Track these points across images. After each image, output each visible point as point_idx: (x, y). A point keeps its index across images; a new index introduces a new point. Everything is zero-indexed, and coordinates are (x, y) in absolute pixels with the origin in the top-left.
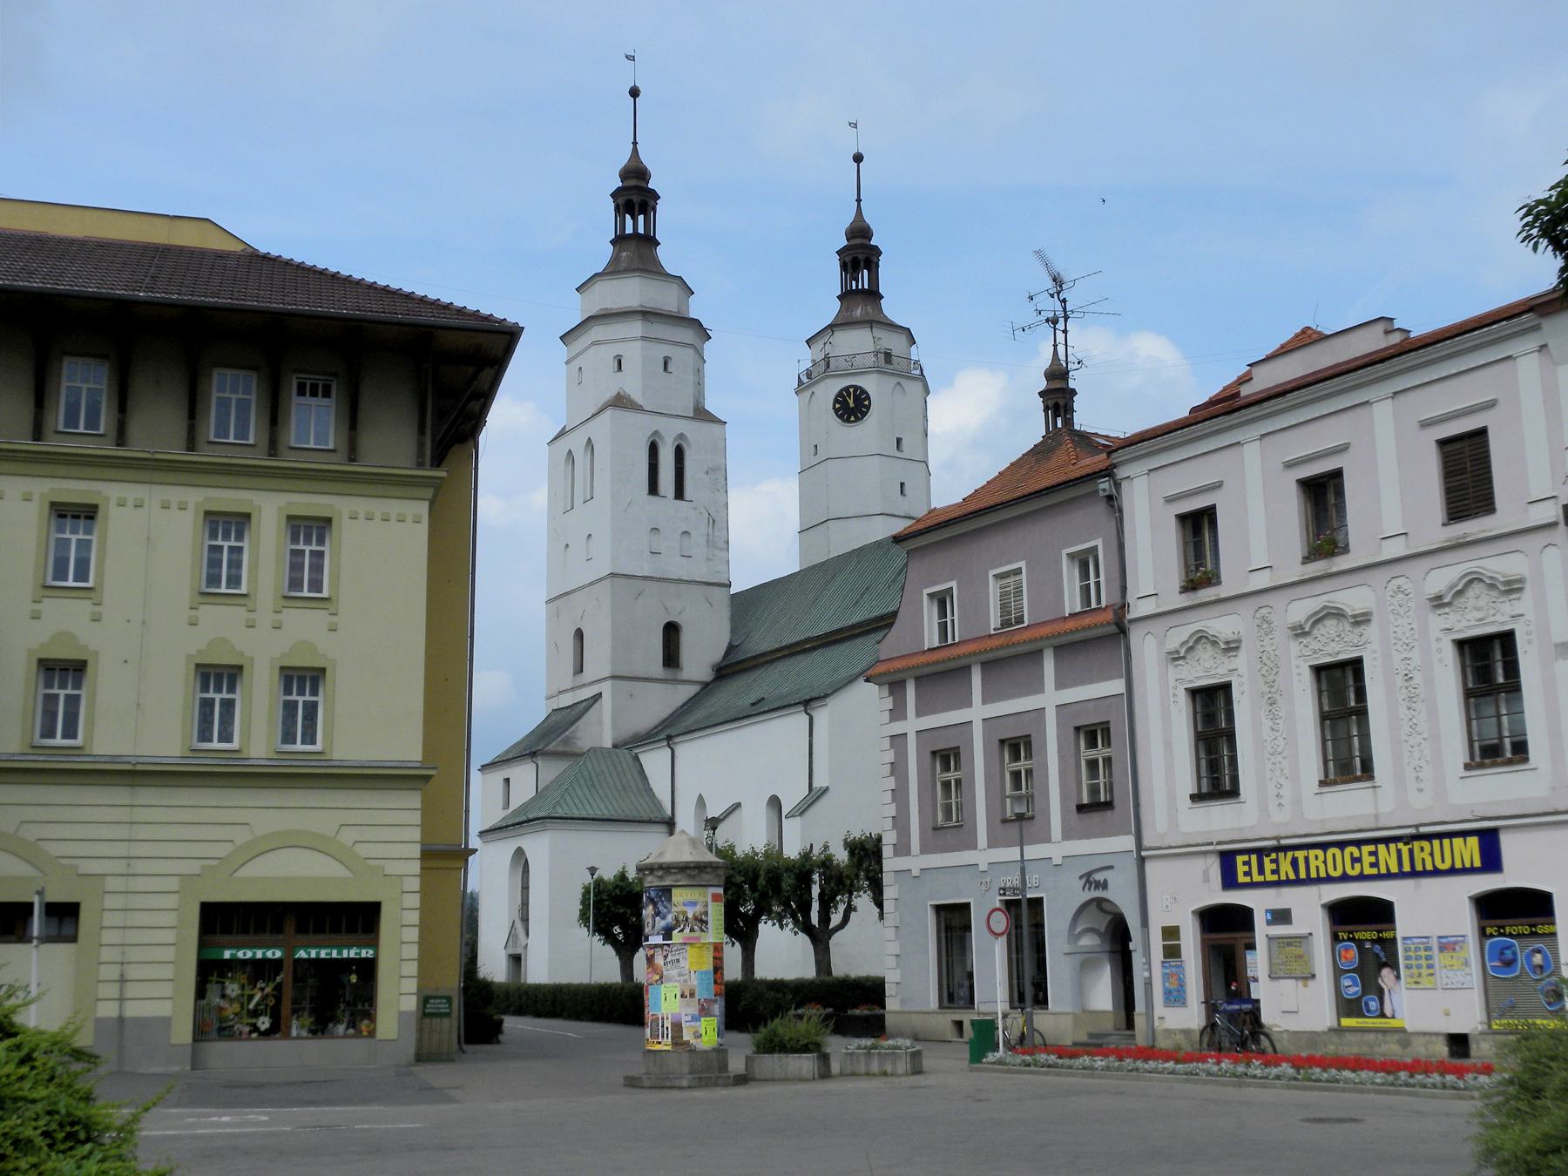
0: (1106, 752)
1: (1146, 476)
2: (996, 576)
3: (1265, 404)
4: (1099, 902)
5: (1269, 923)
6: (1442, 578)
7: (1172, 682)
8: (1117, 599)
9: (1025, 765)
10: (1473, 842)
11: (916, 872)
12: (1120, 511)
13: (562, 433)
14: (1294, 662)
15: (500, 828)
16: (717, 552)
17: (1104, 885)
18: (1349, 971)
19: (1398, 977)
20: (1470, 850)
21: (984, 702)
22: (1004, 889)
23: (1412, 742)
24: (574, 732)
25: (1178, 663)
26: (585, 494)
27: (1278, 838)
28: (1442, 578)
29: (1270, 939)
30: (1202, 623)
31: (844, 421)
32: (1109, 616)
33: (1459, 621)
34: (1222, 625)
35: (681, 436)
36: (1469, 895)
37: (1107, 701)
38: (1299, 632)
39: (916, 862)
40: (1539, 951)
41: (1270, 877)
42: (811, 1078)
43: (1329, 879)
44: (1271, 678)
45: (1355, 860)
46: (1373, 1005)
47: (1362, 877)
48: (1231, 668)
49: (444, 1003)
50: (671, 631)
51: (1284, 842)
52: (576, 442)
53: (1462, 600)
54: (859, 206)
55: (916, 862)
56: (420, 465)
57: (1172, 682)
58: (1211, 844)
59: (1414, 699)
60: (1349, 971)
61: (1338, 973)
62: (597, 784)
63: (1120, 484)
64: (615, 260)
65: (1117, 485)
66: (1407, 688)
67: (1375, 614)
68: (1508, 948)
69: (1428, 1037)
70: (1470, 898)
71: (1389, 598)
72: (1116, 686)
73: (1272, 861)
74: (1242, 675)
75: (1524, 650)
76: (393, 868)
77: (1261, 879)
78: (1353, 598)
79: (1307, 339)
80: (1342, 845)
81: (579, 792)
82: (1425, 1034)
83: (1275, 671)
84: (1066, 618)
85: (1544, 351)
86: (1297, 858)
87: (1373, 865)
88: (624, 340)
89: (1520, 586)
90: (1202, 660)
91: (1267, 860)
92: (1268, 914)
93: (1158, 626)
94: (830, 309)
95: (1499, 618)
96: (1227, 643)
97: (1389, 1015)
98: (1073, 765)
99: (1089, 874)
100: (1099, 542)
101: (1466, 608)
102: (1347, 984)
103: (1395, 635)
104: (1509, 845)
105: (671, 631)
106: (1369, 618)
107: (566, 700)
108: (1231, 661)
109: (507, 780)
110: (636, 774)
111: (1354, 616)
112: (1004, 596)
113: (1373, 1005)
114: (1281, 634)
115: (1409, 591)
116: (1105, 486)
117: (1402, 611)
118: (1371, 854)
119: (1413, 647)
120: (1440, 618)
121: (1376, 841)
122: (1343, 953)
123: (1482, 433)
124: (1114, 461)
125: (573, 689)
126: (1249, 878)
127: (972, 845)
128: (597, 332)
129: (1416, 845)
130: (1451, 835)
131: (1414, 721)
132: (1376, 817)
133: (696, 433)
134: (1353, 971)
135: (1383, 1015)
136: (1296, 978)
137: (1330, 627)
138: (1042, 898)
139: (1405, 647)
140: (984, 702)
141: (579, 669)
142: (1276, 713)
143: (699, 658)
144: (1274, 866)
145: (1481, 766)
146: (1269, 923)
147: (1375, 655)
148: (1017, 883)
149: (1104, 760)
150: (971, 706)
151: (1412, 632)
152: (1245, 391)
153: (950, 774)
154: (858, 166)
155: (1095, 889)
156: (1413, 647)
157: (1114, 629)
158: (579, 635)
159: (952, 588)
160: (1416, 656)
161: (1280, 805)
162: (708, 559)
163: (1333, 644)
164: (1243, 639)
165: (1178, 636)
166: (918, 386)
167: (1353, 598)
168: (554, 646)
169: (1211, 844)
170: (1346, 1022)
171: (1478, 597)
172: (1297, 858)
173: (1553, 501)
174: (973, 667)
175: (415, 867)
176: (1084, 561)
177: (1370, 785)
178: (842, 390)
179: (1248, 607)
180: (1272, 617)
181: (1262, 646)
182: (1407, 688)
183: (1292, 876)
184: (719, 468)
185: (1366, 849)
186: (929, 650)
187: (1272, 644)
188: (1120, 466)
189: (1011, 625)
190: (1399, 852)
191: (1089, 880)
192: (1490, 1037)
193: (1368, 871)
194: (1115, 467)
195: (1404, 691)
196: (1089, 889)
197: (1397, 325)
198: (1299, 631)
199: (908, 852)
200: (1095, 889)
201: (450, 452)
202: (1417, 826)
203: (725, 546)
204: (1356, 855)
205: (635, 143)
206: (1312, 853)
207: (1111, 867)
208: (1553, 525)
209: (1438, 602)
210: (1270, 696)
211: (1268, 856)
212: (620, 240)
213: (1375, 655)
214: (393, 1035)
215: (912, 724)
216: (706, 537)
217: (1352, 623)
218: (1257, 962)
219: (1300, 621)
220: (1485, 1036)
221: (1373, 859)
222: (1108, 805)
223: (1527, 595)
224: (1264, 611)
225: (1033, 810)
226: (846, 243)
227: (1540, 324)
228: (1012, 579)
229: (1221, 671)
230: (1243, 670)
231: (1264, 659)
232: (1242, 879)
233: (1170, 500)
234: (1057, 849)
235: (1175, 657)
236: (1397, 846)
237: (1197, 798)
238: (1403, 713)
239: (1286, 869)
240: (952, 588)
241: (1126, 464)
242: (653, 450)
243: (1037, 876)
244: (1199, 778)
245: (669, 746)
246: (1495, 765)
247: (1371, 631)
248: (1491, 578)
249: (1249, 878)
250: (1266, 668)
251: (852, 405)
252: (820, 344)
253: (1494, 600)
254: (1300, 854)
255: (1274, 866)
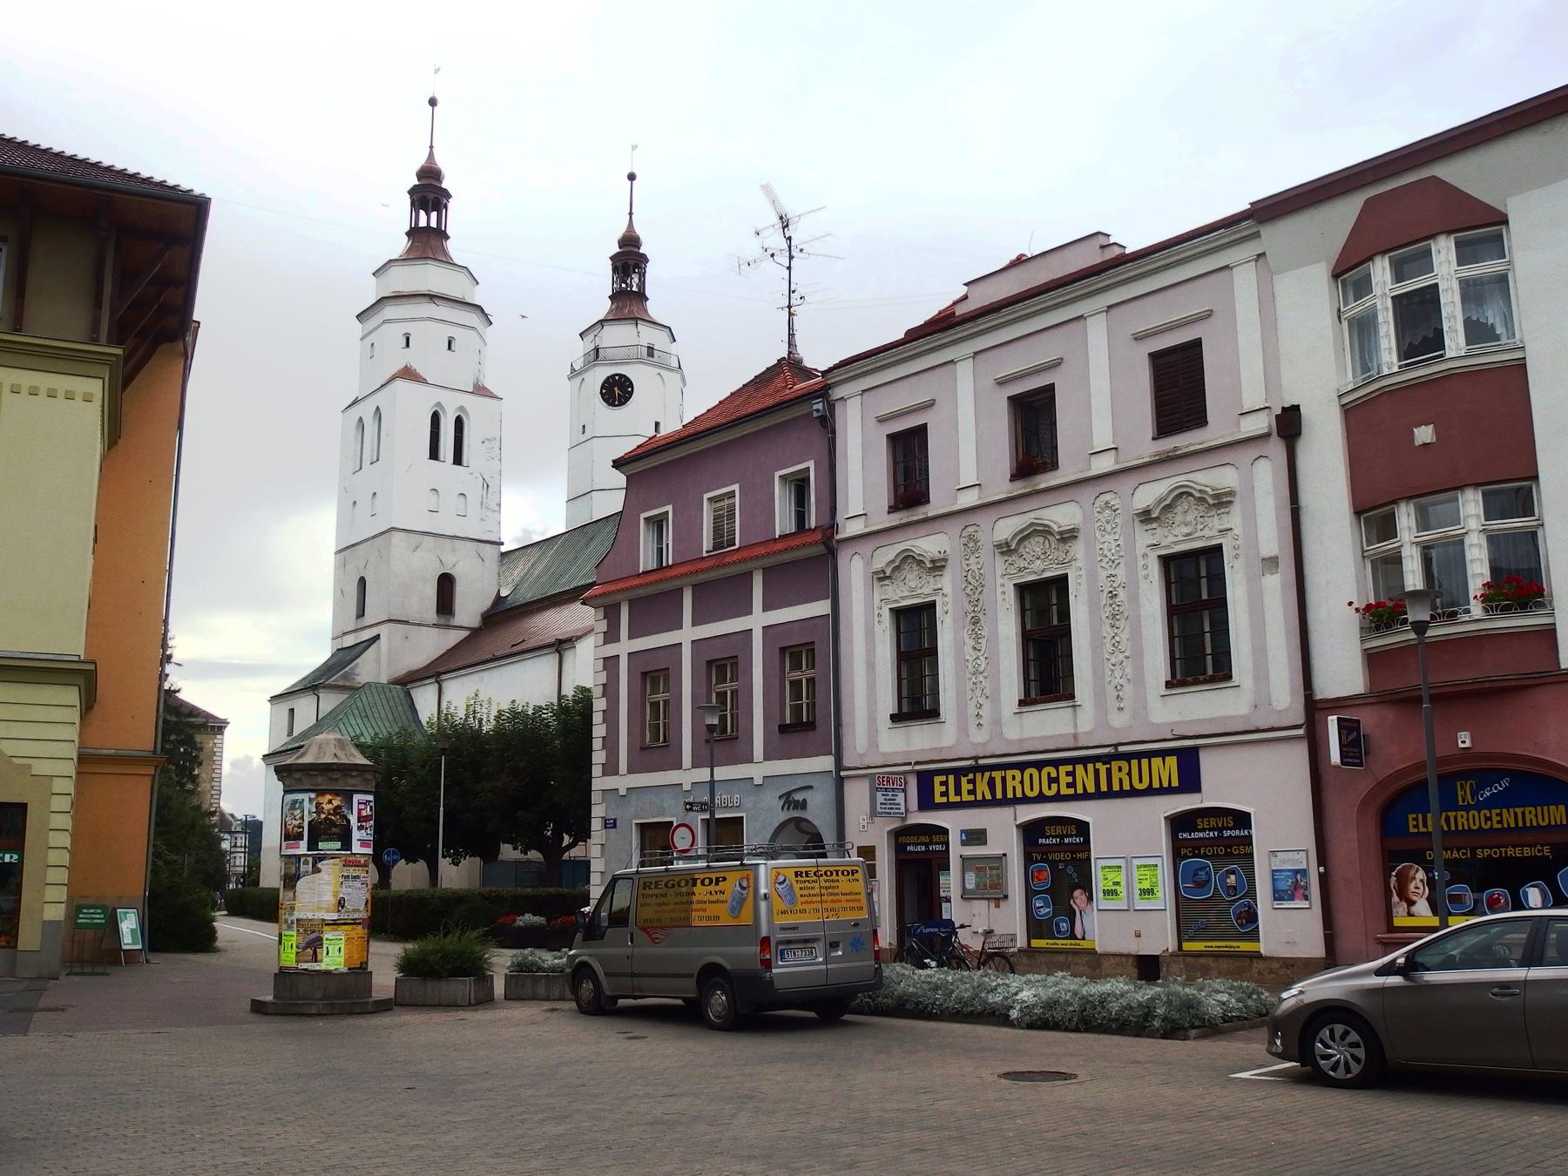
0: (810, 673)
1: (860, 397)
2: (710, 499)
3: (981, 320)
4: (798, 822)
5: (964, 843)
6: (1149, 494)
7: (877, 602)
8: (826, 521)
9: (732, 686)
10: (1172, 761)
11: (622, 792)
12: (834, 432)
13: (355, 402)
14: (999, 581)
15: (280, 752)
16: (489, 513)
17: (803, 805)
18: (1040, 892)
19: (1090, 898)
20: (1168, 770)
21: (694, 624)
22: (691, 804)
23: (1113, 660)
24: (355, 667)
25: (884, 583)
26: (372, 456)
27: (976, 758)
28: (1149, 494)
29: (964, 859)
30: (909, 543)
31: (609, 404)
32: (818, 536)
33: (1166, 537)
34: (929, 545)
35: (462, 408)
36: (1166, 815)
37: (812, 622)
38: (1005, 549)
39: (624, 782)
40: (1233, 872)
41: (966, 797)
42: (467, 1003)
43: (1026, 800)
44: (976, 597)
45: (1051, 780)
46: (1064, 926)
47: (1058, 798)
48: (936, 587)
49: (100, 914)
50: (446, 584)
51: (981, 762)
52: (366, 410)
53: (1170, 515)
54: (631, 217)
55: (624, 782)
56: (94, 340)
57: (877, 602)
58: (910, 764)
59: (1118, 617)
60: (1040, 892)
61: (1030, 894)
62: (370, 715)
63: (834, 406)
64: (409, 250)
65: (831, 407)
66: (1111, 605)
67: (1082, 532)
68: (1202, 869)
69: (1117, 959)
70: (1166, 818)
71: (1096, 515)
72: (821, 608)
73: (969, 782)
74: (947, 594)
75: (1231, 564)
76: (40, 768)
77: (958, 799)
78: (1061, 515)
79: (1020, 261)
80: (1039, 765)
81: (353, 722)
82: (1114, 955)
83: (980, 589)
84: (776, 539)
85: (1261, 261)
86: (994, 778)
87: (1069, 785)
88: (413, 320)
89: (1229, 499)
90: (907, 579)
91: (964, 780)
92: (963, 835)
93: (866, 547)
94: (603, 307)
95: (1207, 532)
96: (933, 561)
97: (1079, 937)
98: (777, 685)
99: (789, 794)
100: (811, 464)
101: (1173, 523)
102: (1038, 905)
103: (1101, 552)
104: (1210, 765)
105: (446, 584)
106: (1075, 534)
107: (349, 641)
108: (936, 581)
109: (292, 711)
110: (407, 707)
111: (1061, 533)
112: (717, 520)
113: (1064, 926)
114: (986, 551)
115: (1117, 507)
116: (820, 406)
117: (1109, 528)
118: (1068, 774)
119: (1119, 563)
120: (1146, 534)
121: (1073, 761)
122: (1036, 874)
123: (1197, 344)
124: (829, 382)
125: (355, 631)
126: (946, 798)
127: (678, 765)
128: (390, 311)
129: (1115, 765)
130: (1150, 754)
131: (1117, 639)
132: (1075, 736)
133: (476, 409)
134: (1045, 892)
135: (1073, 937)
136: (988, 899)
137: (1035, 545)
138: (742, 818)
139: (1110, 564)
140: (694, 624)
141: (361, 613)
142: (980, 632)
143: (469, 610)
144: (971, 787)
145: (1183, 684)
146: (964, 843)
147: (1080, 573)
148: (706, 798)
149: (807, 680)
150: (682, 628)
151: (1118, 548)
152: (960, 310)
153: (658, 696)
154: (632, 184)
155: (793, 809)
156: (1119, 563)
157: (821, 549)
158: (362, 582)
159: (667, 512)
160: (1121, 572)
161: (979, 724)
162: (482, 519)
163: (1039, 562)
164: (949, 558)
165: (886, 555)
166: (676, 377)
167: (1061, 515)
168: (340, 592)
169: (910, 764)
170: (1036, 943)
171: (1186, 515)
172: (994, 778)
173: (1267, 411)
174: (684, 589)
175: (70, 768)
176: (799, 485)
177: (1071, 704)
178: (608, 378)
179: (954, 528)
180: (979, 535)
181: (968, 565)
182: (1111, 605)
183: (988, 796)
184: (495, 439)
185: (1063, 769)
186: (644, 573)
187: (978, 563)
188: (834, 387)
189: (723, 547)
190: (1097, 772)
191: (788, 801)
192: (1181, 959)
193: (1065, 791)
194: (830, 388)
195: (1108, 609)
196: (788, 809)
197: (1112, 240)
198: (1005, 549)
199: (616, 773)
200: (793, 809)
201: (158, 350)
202: (1116, 746)
203: (497, 508)
204: (1054, 775)
205: (431, 147)
206: (1009, 773)
207: (811, 787)
208: (1266, 436)
209: (1146, 517)
210: (973, 615)
211: (965, 776)
212: (414, 232)
213: (1080, 573)
214: (35, 946)
215: (624, 647)
216: (480, 500)
217: (1058, 540)
218: (951, 882)
219: (1007, 539)
220: (1174, 958)
221: (1070, 779)
222: (811, 726)
223: (1236, 509)
224: (970, 529)
225: (737, 732)
226: (618, 250)
227: (1259, 232)
228: (727, 502)
229: (926, 590)
230: (948, 589)
231: (969, 578)
232: (938, 799)
233: (882, 420)
234: (758, 770)
235: (882, 577)
236: (1094, 766)
237: (895, 718)
238: (1107, 630)
239: (982, 788)
240: (667, 512)
241: (840, 385)
242: (435, 419)
243: (738, 796)
244: (900, 698)
245: (437, 681)
246: (1196, 682)
247: (1078, 549)
248: (1200, 491)
249: (946, 798)
250: (971, 587)
251: (616, 389)
252: (591, 337)
253: (1202, 514)
254: (997, 775)
255: (971, 787)
